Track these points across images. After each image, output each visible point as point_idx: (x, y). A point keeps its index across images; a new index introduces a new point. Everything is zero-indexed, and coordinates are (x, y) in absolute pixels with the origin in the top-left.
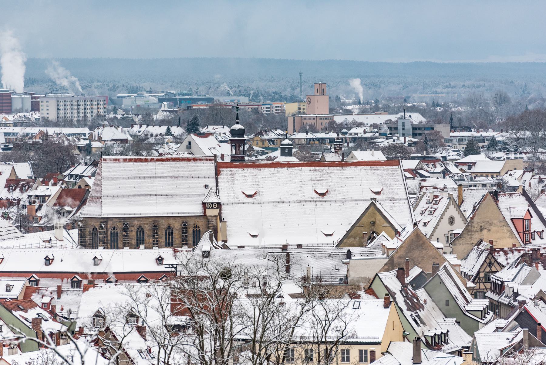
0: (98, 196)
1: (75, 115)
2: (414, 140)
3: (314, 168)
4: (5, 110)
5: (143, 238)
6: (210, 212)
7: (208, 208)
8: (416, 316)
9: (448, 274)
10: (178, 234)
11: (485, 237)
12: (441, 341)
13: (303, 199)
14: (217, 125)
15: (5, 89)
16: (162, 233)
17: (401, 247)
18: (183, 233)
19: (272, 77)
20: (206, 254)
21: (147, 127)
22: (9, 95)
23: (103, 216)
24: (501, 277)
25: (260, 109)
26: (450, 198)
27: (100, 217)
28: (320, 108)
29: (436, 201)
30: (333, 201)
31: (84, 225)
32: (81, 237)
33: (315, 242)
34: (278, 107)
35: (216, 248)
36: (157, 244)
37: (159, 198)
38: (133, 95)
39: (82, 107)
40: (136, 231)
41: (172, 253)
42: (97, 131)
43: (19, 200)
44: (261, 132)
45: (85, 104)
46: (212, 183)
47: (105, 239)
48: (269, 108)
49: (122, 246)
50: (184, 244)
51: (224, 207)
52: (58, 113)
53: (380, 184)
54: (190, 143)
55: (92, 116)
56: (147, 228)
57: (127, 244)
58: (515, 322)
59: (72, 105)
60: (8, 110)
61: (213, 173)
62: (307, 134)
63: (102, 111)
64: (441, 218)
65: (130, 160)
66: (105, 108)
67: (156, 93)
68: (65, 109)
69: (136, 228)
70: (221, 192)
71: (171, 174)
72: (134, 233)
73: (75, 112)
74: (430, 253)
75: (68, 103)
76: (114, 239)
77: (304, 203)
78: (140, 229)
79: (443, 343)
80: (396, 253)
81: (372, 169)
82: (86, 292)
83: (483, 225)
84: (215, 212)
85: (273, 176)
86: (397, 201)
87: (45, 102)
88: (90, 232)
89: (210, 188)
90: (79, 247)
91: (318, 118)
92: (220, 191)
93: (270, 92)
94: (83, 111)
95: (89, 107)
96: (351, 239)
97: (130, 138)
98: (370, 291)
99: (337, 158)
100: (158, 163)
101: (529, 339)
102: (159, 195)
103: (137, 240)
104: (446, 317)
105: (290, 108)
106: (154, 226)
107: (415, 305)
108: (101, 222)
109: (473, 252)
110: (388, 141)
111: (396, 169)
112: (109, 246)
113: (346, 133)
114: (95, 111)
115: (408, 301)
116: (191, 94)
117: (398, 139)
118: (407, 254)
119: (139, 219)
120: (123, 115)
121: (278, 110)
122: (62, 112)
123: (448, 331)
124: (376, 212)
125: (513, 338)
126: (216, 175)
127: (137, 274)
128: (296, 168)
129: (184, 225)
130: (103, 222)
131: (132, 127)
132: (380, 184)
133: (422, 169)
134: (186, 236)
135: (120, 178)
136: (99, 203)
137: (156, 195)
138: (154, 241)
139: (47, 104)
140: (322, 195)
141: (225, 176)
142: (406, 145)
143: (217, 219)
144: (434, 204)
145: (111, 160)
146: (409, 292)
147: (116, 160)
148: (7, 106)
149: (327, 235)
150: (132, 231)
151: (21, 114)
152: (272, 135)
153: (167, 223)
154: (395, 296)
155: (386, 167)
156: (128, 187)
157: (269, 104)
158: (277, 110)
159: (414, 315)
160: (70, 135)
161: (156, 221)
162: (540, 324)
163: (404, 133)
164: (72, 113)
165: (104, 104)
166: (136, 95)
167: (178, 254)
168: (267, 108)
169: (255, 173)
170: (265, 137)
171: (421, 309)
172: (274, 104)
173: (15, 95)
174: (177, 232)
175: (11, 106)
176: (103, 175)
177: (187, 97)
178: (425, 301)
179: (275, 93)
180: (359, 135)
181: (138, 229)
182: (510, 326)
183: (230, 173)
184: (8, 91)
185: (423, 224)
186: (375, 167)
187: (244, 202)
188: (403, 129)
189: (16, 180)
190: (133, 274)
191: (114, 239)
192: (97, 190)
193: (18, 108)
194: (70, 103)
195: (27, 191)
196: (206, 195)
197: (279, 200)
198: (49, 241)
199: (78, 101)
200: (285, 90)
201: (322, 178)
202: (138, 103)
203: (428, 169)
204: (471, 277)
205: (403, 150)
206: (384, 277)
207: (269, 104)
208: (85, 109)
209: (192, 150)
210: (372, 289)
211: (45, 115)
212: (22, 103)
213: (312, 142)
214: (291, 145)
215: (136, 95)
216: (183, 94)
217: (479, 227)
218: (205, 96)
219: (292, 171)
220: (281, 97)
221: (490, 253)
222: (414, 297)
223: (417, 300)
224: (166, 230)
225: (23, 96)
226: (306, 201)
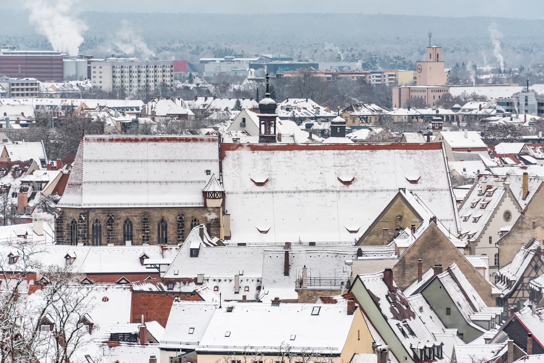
0: (78, 182)
1: (135, 84)
2: (537, 118)
3: (338, 151)
4: (55, 77)
5: (131, 232)
6: (211, 203)
7: (209, 198)
8: (405, 325)
9: (452, 277)
10: (173, 229)
11: (538, 235)
12: (434, 355)
13: (323, 188)
14: (300, 98)
15: (56, 51)
16: (154, 227)
17: (414, 245)
18: (178, 228)
19: (398, 38)
20: (194, 253)
21: (214, 99)
22: (61, 59)
23: (83, 207)
24: (540, 283)
25: (368, 79)
26: (505, 189)
27: (80, 207)
28: (436, 77)
29: (490, 193)
30: (360, 191)
31: (61, 217)
32: (57, 231)
33: (337, 240)
34: (392, 75)
35: (207, 245)
36: (148, 240)
37: (151, 186)
38: (218, 60)
39: (143, 75)
40: (122, 224)
41: (159, 252)
42: (150, 104)
43: (8, 188)
44: (351, 107)
45: (147, 71)
46: (215, 169)
47: (86, 234)
48: (379, 77)
49: (105, 242)
50: (180, 241)
51: (228, 197)
52: (114, 82)
53: (418, 171)
54: (244, 120)
55: (155, 85)
56: (136, 220)
57: (112, 239)
58: (503, 332)
59: (131, 72)
60: (60, 77)
61: (216, 156)
62: (409, 110)
63: (168, 79)
64: (495, 212)
65: (118, 140)
66: (172, 76)
67: (248, 57)
68: (122, 77)
69: (123, 221)
70: (225, 179)
71: (166, 158)
72: (120, 227)
73: (135, 80)
74: (449, 254)
75: (127, 70)
76: (97, 234)
77: (325, 193)
78: (128, 222)
79: (436, 358)
80: (408, 252)
81: (408, 154)
82: (33, 295)
83: (536, 221)
84: (217, 203)
85: (288, 160)
86: (437, 192)
87: (98, 67)
88: (68, 225)
89: (212, 174)
90: (56, 243)
91: (430, 90)
92: (224, 177)
93: (391, 57)
94: (145, 79)
95: (152, 74)
96: (374, 237)
97: (191, 113)
98: (349, 295)
99: (421, 140)
100: (151, 143)
101: (514, 352)
102: (151, 182)
103: (124, 235)
104: (446, 327)
105: (405, 77)
106: (145, 219)
107: (403, 312)
108: (81, 214)
109: (519, 253)
110: (505, 119)
111: (437, 153)
112: (90, 242)
113: (459, 109)
114: (160, 80)
115: (395, 308)
116: (291, 59)
117: (517, 117)
118: (421, 253)
119: (126, 210)
120: (198, 85)
121: (392, 79)
122: (118, 80)
123: (442, 344)
124: (404, 204)
125: (499, 351)
126: (220, 158)
127: (115, 276)
128: (317, 151)
129: (181, 218)
130: (84, 214)
131: (196, 99)
132: (418, 171)
133: (527, 154)
134: (183, 231)
135: (105, 161)
136: (79, 190)
137: (147, 182)
138: (144, 237)
139: (101, 70)
140: (347, 183)
141: (230, 160)
142: (526, 124)
143: (219, 212)
144: (487, 196)
145: (94, 140)
146: (397, 297)
147: (101, 140)
148: (58, 73)
149: (351, 232)
150: (118, 224)
151: (74, 83)
152: (364, 111)
153: (159, 215)
154: (379, 302)
155: (425, 151)
156: (115, 172)
157: (380, 73)
158: (390, 79)
159: (401, 324)
160: (113, 109)
161: (147, 213)
162: (531, 335)
163: (526, 109)
164: (131, 81)
165: (172, 71)
166: (223, 59)
167: (166, 252)
168: (377, 77)
169: (267, 157)
170: (356, 113)
171: (411, 318)
172: (387, 72)
173: (67, 58)
174: (172, 226)
175: (62, 73)
176: (85, 157)
177: (287, 62)
178: (421, 309)
179: (398, 58)
180: (474, 112)
181: (126, 222)
182: (498, 337)
183: (237, 156)
184: (59, 54)
185: (473, 220)
186: (412, 151)
187: (253, 191)
188: (526, 104)
189: (7, 163)
190: (112, 276)
191: (97, 234)
192: (77, 175)
193: (71, 75)
194: (128, 70)
195: (20, 176)
196: (207, 183)
197: (295, 190)
198: (25, 237)
199: (139, 66)
200: (411, 54)
201: (347, 163)
202: (223, 70)
203: (535, 154)
204: (513, 282)
205: (512, 130)
206: (367, 280)
207: (380, 73)
208: (147, 76)
209: (246, 129)
210: (352, 293)
211: (98, 85)
212: (76, 69)
213: (415, 120)
214: (344, 123)
215: (223, 59)
216: (282, 59)
217: (532, 224)
218: (307, 61)
219: (312, 154)
220: (405, 63)
221: (535, 255)
222: (403, 303)
223: (408, 306)
224: (159, 225)
225: (78, 60)
226: (327, 191)
